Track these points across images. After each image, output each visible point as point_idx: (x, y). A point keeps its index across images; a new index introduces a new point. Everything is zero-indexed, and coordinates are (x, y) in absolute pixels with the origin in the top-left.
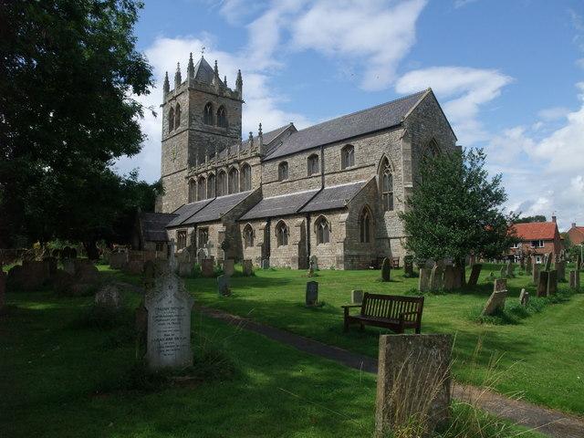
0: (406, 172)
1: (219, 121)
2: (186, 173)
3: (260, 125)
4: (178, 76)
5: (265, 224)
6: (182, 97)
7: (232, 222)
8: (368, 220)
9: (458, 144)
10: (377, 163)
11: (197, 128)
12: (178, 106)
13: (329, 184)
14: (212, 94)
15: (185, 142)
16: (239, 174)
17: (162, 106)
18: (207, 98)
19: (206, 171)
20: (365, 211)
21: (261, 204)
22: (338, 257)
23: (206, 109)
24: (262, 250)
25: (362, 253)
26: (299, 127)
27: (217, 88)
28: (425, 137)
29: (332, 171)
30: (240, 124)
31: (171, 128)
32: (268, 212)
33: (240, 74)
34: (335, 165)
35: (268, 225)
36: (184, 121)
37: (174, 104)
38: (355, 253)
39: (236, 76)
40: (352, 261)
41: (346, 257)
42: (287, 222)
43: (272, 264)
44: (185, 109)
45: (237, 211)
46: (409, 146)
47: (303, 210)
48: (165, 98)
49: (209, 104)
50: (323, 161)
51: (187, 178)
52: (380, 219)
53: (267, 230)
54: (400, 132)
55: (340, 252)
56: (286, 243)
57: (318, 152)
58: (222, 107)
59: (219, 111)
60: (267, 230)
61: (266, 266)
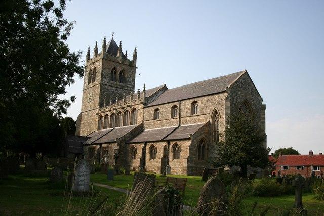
2: (97, 111)
3: (145, 85)
4: (96, 50)
5: (143, 146)
6: (97, 64)
7: (123, 144)
8: (203, 146)
9: (263, 103)
11: (106, 83)
13: (183, 124)
15: (98, 91)
19: (110, 111)
20: (202, 141)
23: (112, 71)
30: (134, 81)
33: (136, 50)
36: (98, 78)
39: (133, 51)
40: (192, 170)
41: (188, 168)
46: (229, 104)
47: (165, 139)
49: (115, 69)
51: (97, 114)
53: (144, 149)
54: (225, 95)
55: (185, 165)
57: (177, 104)
58: (122, 71)
59: (120, 73)
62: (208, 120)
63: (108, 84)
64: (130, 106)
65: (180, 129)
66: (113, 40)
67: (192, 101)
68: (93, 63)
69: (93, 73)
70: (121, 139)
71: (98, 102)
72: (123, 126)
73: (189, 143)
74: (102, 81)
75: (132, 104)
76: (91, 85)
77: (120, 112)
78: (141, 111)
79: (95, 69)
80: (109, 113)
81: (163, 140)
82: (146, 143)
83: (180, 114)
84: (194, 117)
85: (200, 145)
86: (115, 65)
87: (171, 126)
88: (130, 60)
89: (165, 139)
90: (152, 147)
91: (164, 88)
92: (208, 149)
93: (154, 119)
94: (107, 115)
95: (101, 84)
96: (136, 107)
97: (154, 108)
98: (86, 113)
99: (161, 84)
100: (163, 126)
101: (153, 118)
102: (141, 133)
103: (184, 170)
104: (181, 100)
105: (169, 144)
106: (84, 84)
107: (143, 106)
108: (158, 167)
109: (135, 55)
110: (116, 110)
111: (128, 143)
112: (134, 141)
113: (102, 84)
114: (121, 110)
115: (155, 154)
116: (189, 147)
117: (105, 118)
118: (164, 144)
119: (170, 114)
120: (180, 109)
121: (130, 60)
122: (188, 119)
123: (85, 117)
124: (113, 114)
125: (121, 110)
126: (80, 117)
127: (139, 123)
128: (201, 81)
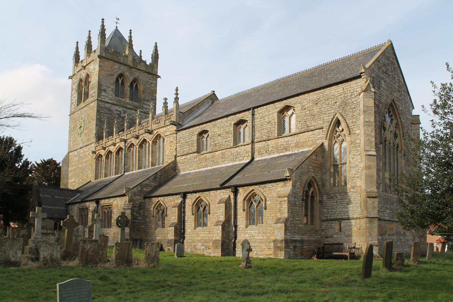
0: (367, 135)
1: (131, 94)
2: (92, 147)
3: (177, 90)
4: (89, 46)
5: (178, 200)
6: (91, 67)
7: (139, 199)
8: (313, 197)
9: (414, 113)
10: (326, 125)
12: (88, 76)
13: (261, 154)
14: (126, 65)
15: (94, 114)
16: (148, 147)
17: (71, 78)
18: (117, 69)
19: (114, 144)
20: (310, 185)
21: (176, 179)
22: (275, 241)
23: (117, 80)
24: (175, 232)
25: (305, 238)
26: (220, 96)
27: (130, 58)
28: (386, 99)
29: (265, 138)
31: (79, 101)
32: (184, 187)
33: (156, 47)
34: (270, 132)
35: (183, 202)
36: (93, 92)
37: (83, 74)
38: (298, 237)
40: (295, 247)
41: (287, 242)
42: (206, 197)
43: (187, 249)
44: (94, 80)
45: (146, 185)
46: (371, 103)
47: (227, 185)
48: (74, 69)
49: (121, 75)
50: (253, 127)
51: (94, 152)
52: (148, 191)
53: (181, 208)
54: (361, 83)
55: (280, 234)
56: (205, 225)
57: (247, 116)
58: (135, 80)
59: (132, 84)
60: (181, 208)
61: (181, 253)
62: (319, 142)
63: (110, 102)
64: (150, 132)
65: (253, 163)
66: (117, 31)
67: (280, 105)
68: (84, 67)
69: (85, 84)
70: (135, 190)
71: (94, 132)
72: (139, 169)
73: (286, 188)
74: (99, 95)
75: (154, 127)
76: (82, 105)
77: (132, 145)
78: (172, 138)
79: (88, 76)
80: (113, 149)
81: (222, 187)
82: (184, 195)
83: (253, 136)
84: (286, 139)
85: (306, 194)
86: (123, 69)
87: (234, 160)
88: (148, 63)
89: (227, 185)
90: (198, 204)
91: (213, 97)
92: (321, 202)
93: (198, 151)
94: (110, 152)
95: (98, 100)
96: (161, 131)
97: (198, 129)
98: (76, 153)
99: (208, 92)
100: (218, 163)
101: (195, 149)
102: (173, 177)
103: (276, 248)
104: (254, 108)
105: (236, 193)
106: (72, 104)
107: (174, 128)
108: (215, 242)
109: (155, 57)
110: (125, 141)
111: (148, 196)
112: (161, 191)
113: (101, 101)
114: (134, 141)
115: (205, 216)
116: (288, 197)
117: (107, 157)
118: (226, 194)
119: (231, 138)
120: (253, 127)
121: (148, 63)
122: (271, 143)
123: (74, 159)
124: (120, 149)
125: (134, 141)
126: (66, 160)
127: (168, 160)
128: (275, 79)
